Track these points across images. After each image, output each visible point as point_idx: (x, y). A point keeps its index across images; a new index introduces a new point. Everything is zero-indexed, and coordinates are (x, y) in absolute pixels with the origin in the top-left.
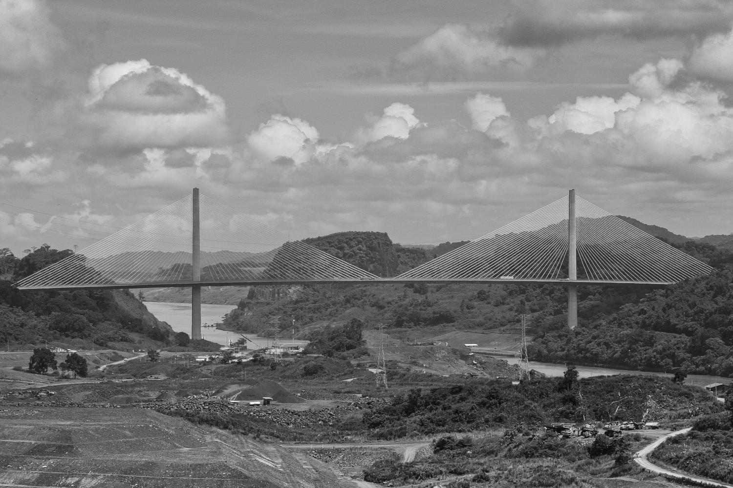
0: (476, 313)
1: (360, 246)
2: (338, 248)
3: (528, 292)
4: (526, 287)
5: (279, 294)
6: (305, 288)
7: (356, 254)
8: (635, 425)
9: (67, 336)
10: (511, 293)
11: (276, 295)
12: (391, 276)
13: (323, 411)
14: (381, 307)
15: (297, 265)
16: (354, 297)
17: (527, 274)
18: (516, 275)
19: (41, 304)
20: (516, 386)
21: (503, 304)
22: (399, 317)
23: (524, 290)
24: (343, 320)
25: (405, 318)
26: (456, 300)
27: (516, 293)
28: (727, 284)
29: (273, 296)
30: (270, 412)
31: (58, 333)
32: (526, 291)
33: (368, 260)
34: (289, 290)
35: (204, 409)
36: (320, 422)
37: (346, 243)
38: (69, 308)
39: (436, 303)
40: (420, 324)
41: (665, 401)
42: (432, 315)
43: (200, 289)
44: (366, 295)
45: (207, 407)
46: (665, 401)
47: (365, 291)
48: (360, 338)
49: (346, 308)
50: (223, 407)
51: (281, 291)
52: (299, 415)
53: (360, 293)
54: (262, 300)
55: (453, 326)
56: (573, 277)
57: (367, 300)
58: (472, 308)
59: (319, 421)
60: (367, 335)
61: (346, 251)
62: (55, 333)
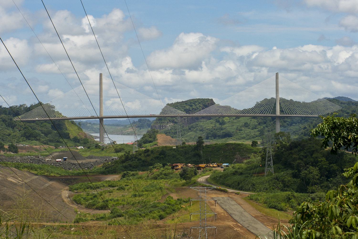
0: (242, 133)
1: (200, 105)
2: (190, 106)
3: (267, 123)
4: (266, 121)
5: (163, 127)
6: (174, 124)
8: (217, 165)
9: (29, 139)
10: (259, 124)
11: (162, 127)
12: (192, 114)
13: (88, 163)
17: (256, 112)
18: (230, 107)
19: (22, 126)
20: (174, 149)
21: (256, 128)
23: (266, 122)
24: (187, 137)
25: (210, 135)
26: (234, 127)
27: (262, 124)
28: (343, 114)
29: (160, 128)
30: (61, 164)
31: (25, 138)
32: (266, 123)
34: (167, 125)
35: (30, 162)
36: (86, 169)
37: (194, 103)
38: (36, 128)
39: (225, 128)
40: (216, 138)
41: (244, 155)
42: (222, 134)
43: (103, 120)
45: (31, 161)
46: (244, 155)
47: (197, 124)
48: (155, 137)
49: (188, 132)
50: (39, 161)
52: (76, 165)
53: (195, 125)
55: (231, 139)
56: (278, 113)
57: (198, 128)
58: (241, 130)
59: (86, 168)
60: (159, 136)
61: (193, 107)
62: (24, 138)
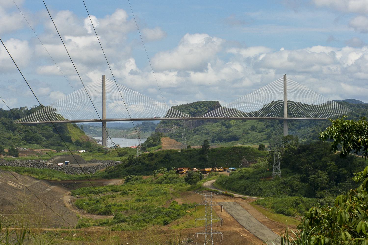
0: (249, 136)
1: (205, 107)
2: (195, 109)
3: (275, 126)
4: (274, 124)
5: (167, 130)
6: (179, 127)
8: (223, 169)
9: (30, 143)
10: (267, 127)
11: (166, 131)
12: (197, 116)
13: (91, 167)
17: (264, 115)
18: (236, 110)
19: (23, 129)
20: (179, 153)
21: (263, 132)
23: (273, 125)
24: (192, 141)
25: (216, 139)
26: (241, 130)
27: (269, 127)
28: (353, 117)
29: (165, 131)
30: (63, 168)
31: (26, 141)
32: (274, 126)
34: (172, 128)
35: (31, 166)
36: (88, 173)
37: (199, 106)
38: (37, 131)
39: (232, 131)
40: (222, 141)
41: (251, 159)
42: (228, 137)
43: (106, 123)
45: (32, 165)
46: (251, 159)
47: (203, 127)
48: (159, 141)
49: (193, 135)
50: (40, 165)
52: (78, 169)
53: (201, 128)
55: (238, 142)
56: (286, 116)
57: (204, 132)
58: (248, 134)
59: (88, 172)
60: (163, 140)
61: (199, 110)
62: (24, 142)
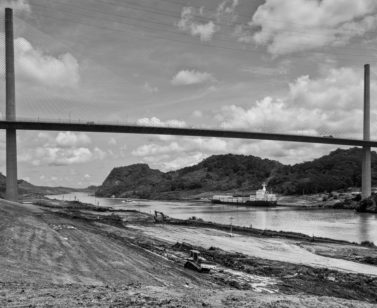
5: (112, 184)
7: (138, 170)
14: (154, 185)
15: (118, 174)
16: (142, 181)
22: (173, 186)
33: (142, 173)
37: (135, 167)
44: (147, 181)
51: (113, 182)
54: (106, 185)
